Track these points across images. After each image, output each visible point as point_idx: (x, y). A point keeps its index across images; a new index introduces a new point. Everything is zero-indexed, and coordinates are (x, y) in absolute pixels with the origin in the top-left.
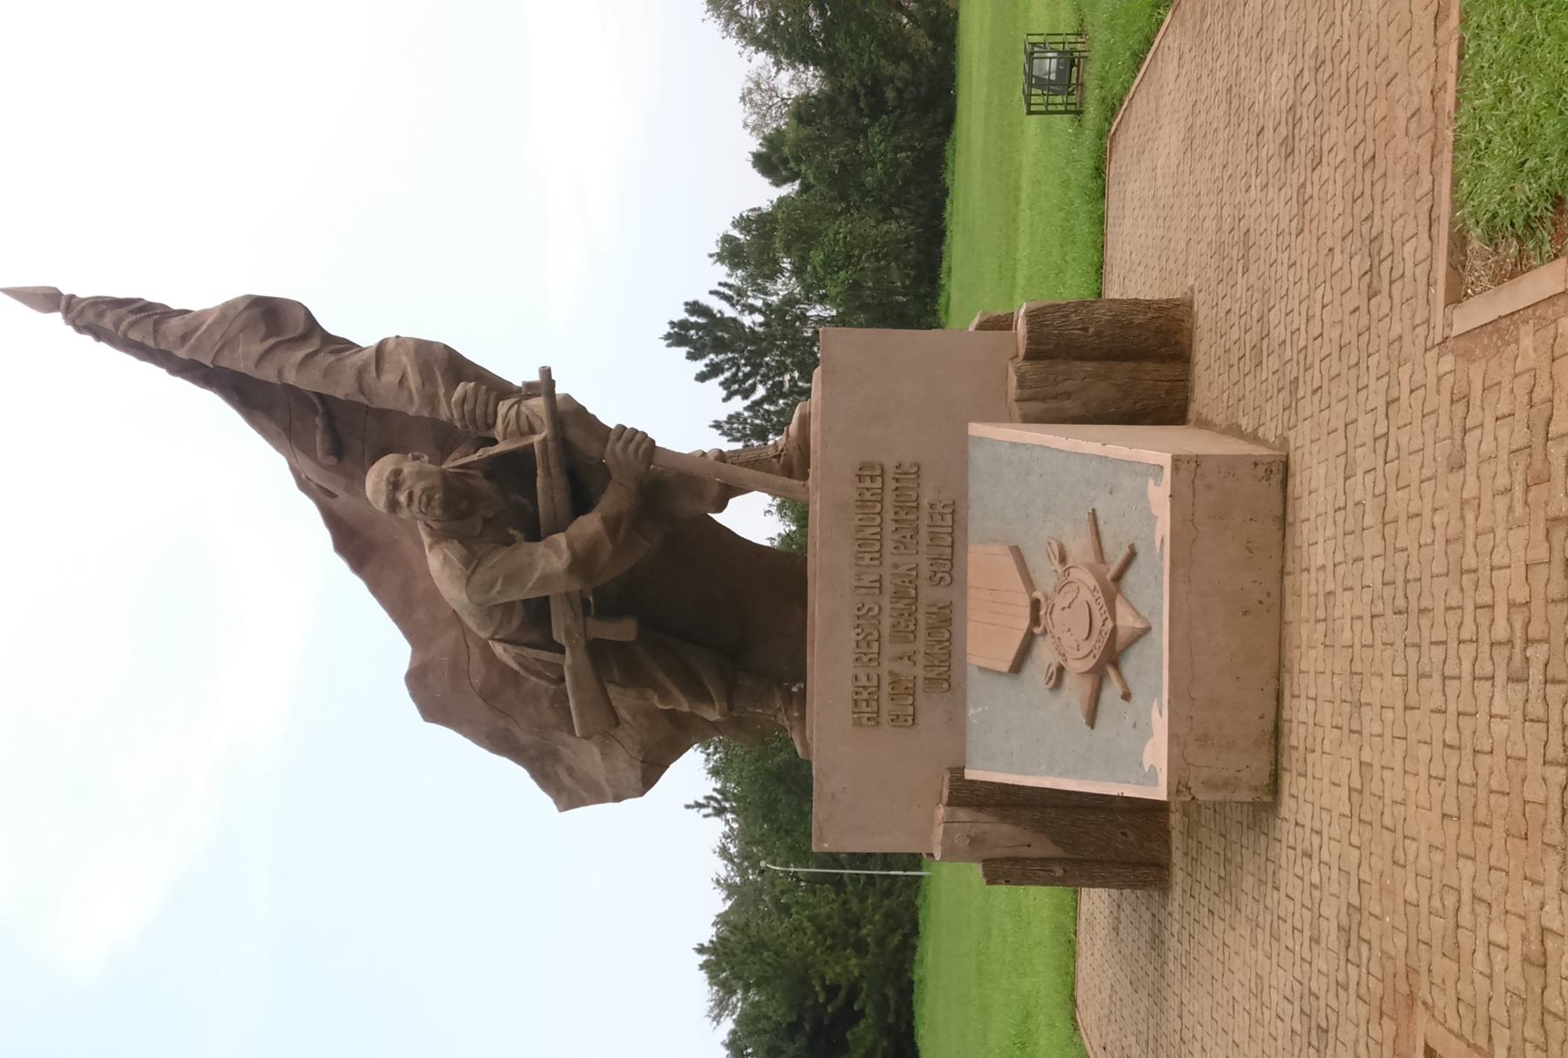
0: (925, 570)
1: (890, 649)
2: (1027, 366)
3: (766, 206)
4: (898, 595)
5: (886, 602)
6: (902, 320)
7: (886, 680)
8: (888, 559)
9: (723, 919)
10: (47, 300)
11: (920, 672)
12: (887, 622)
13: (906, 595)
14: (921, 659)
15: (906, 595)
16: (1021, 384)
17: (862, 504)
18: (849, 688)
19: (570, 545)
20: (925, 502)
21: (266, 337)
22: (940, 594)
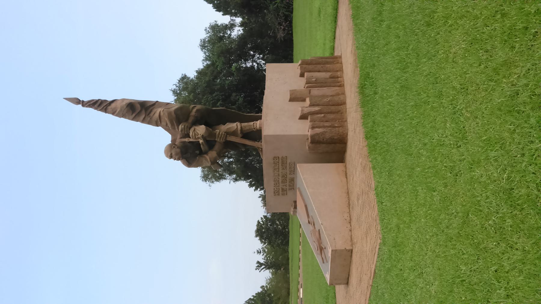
0: (288, 172)
1: (281, 184)
2: (310, 145)
3: (260, 292)
4: (283, 177)
5: (280, 177)
6: (274, 213)
7: (280, 189)
8: (281, 171)
9: (258, 294)
10: (77, 101)
11: (288, 187)
12: (280, 181)
13: (284, 176)
14: (288, 186)
15: (284, 176)
16: (309, 148)
17: (274, 163)
18: (273, 190)
19: (210, 159)
20: (288, 162)
21: (132, 114)
22: (292, 176)
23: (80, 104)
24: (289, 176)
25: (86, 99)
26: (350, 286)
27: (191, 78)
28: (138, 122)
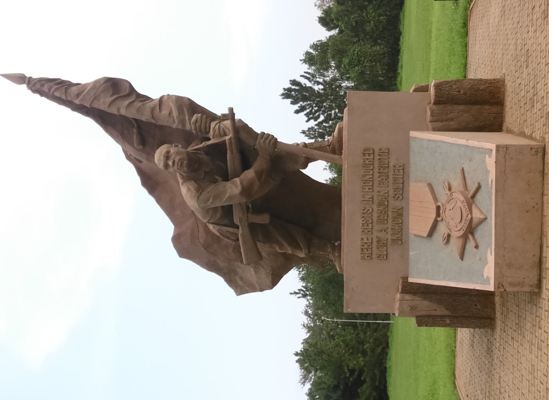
0: (391, 193)
1: (377, 227)
2: (434, 107)
4: (380, 204)
5: (375, 207)
7: (375, 240)
8: (376, 189)
11: (389, 237)
13: (383, 204)
14: (389, 231)
15: (383, 204)
17: (365, 165)
18: (359, 243)
20: (391, 165)
22: (398, 204)
23: (23, 82)
24: (393, 203)
25: (36, 74)
26: (427, 185)
27: (310, 387)
28: (131, 168)
